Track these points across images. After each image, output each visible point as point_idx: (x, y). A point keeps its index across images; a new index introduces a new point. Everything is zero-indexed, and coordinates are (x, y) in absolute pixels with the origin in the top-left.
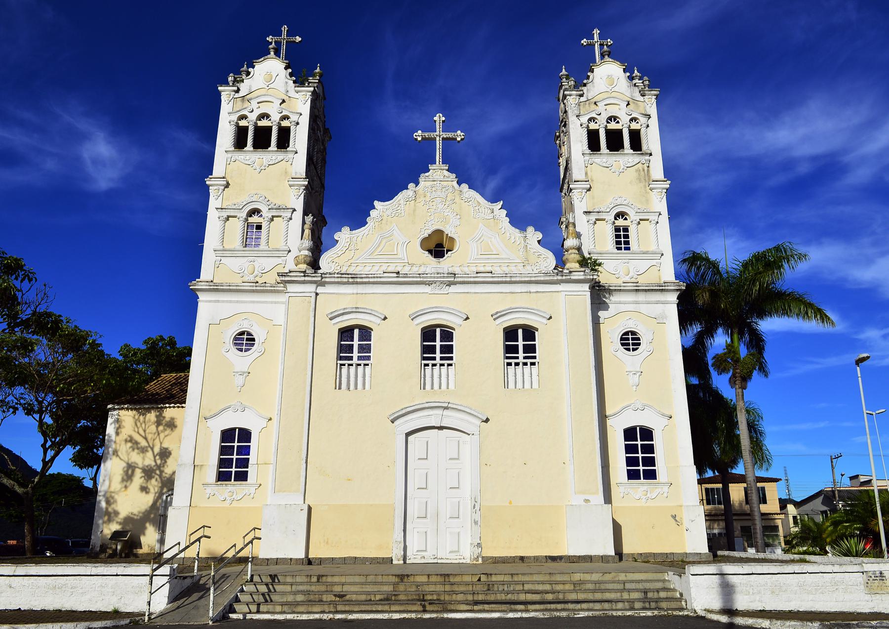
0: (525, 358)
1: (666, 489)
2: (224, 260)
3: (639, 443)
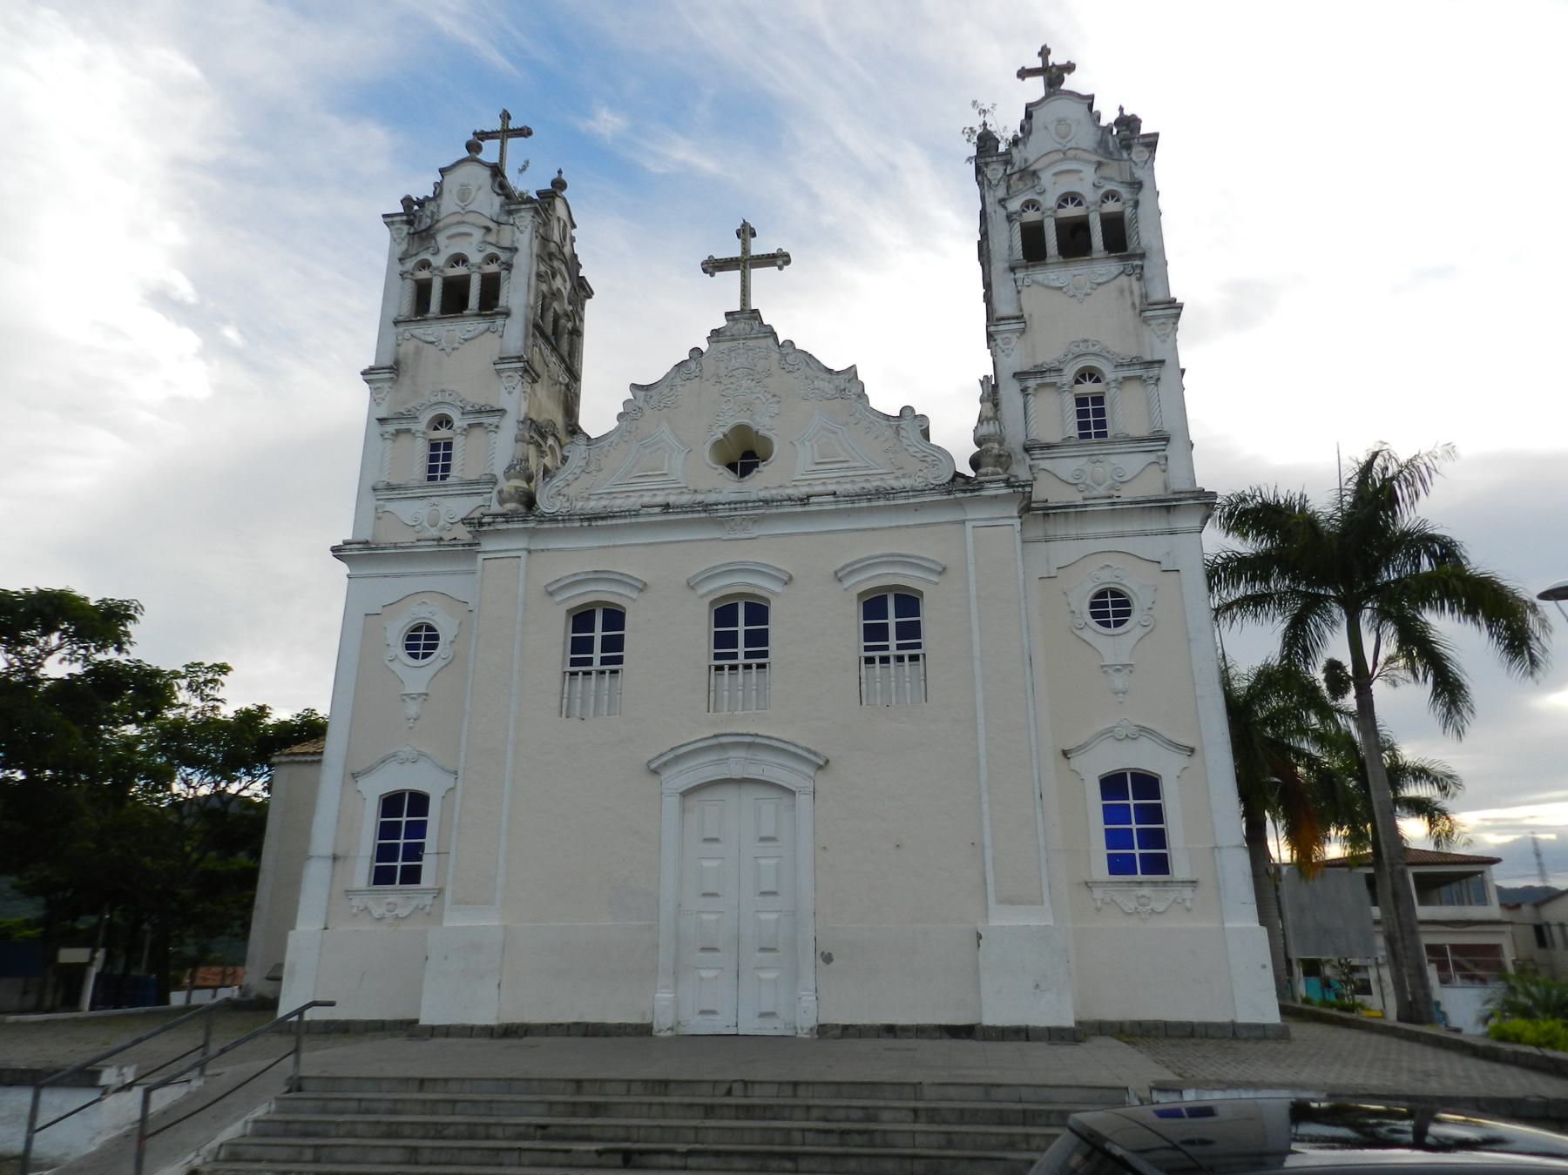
0: (899, 647)
1: (1187, 892)
2: (390, 506)
3: (1132, 802)
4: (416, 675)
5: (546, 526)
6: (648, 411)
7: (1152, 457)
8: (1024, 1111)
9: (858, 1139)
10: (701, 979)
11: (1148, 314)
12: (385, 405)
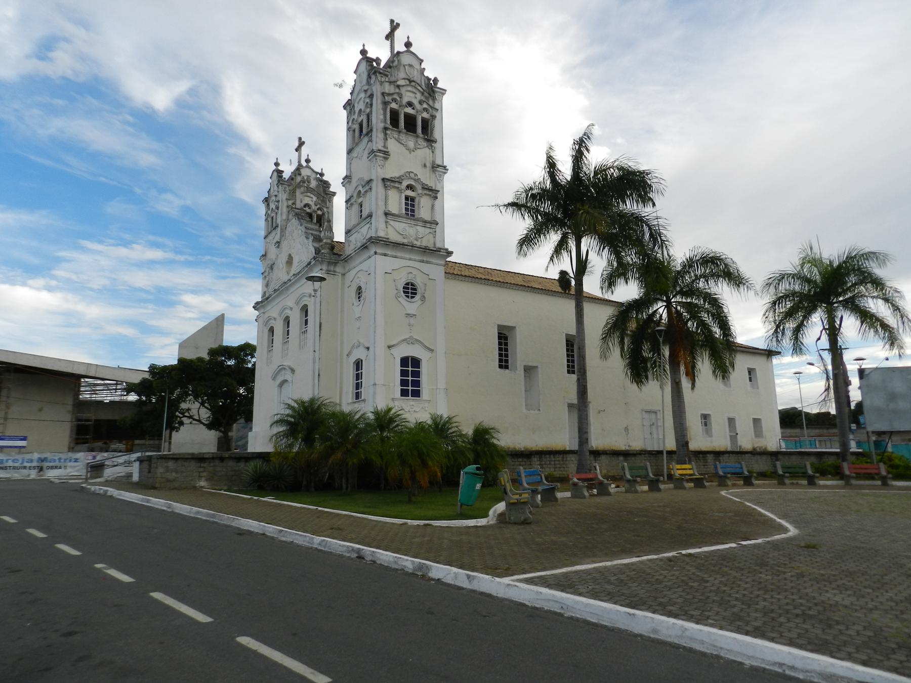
1: (426, 405)
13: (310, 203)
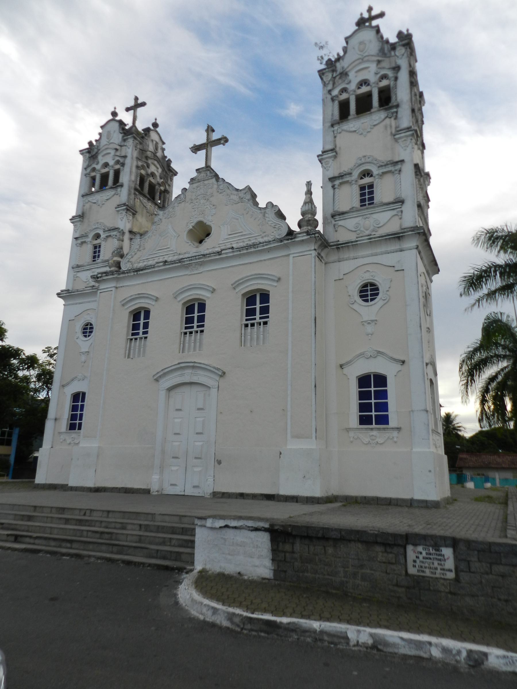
1: (395, 434)
2: (79, 274)
3: (373, 389)
4: (84, 344)
5: (121, 276)
6: (164, 220)
7: (394, 212)
8: (183, 528)
9: (107, 536)
10: (172, 470)
11: (397, 136)
12: (78, 231)
13: (156, 172)
